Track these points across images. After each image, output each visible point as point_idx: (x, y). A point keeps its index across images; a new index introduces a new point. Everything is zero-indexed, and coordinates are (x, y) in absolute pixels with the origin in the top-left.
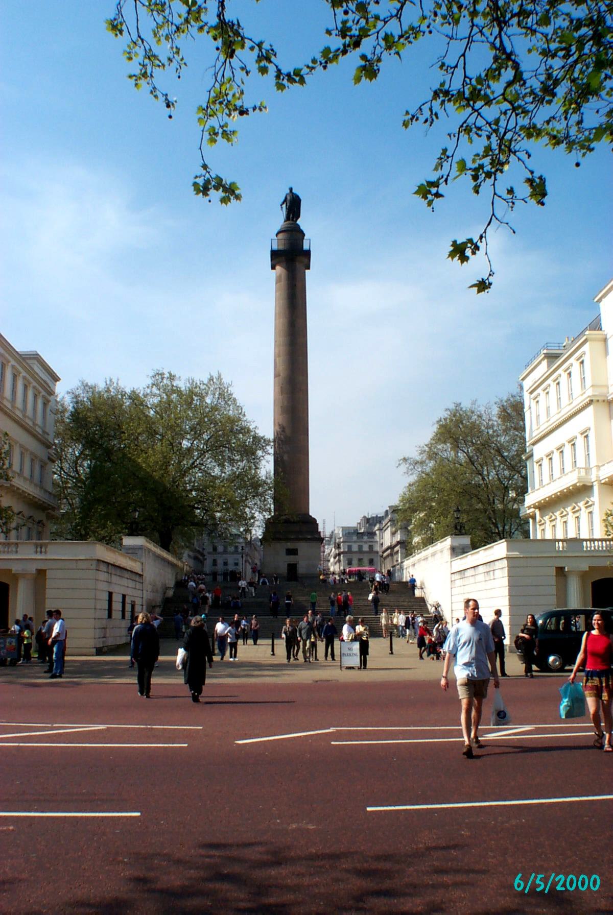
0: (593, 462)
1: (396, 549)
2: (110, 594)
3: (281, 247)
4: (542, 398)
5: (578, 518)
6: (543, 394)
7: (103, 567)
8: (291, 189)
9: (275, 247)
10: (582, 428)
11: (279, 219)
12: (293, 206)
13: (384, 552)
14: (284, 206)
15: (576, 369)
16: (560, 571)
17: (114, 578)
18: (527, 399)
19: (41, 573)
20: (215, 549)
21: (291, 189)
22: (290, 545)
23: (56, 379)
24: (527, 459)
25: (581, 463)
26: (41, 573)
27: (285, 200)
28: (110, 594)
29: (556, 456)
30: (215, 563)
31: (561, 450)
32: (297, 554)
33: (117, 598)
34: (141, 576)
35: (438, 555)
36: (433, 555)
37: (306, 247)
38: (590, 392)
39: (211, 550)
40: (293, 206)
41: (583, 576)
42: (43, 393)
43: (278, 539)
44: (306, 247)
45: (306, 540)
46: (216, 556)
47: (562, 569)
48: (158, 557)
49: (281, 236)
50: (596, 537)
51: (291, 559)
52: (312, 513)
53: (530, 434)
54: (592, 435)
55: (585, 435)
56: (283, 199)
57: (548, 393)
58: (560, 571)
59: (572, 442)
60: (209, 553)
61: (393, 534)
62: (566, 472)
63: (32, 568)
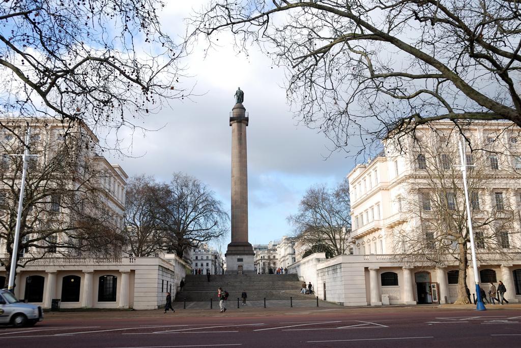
0: (382, 218)
1: (287, 258)
2: (163, 281)
3: (235, 116)
4: (358, 186)
5: (375, 243)
6: (363, 181)
7: (161, 269)
8: (239, 88)
9: (232, 116)
10: (376, 202)
11: (234, 101)
12: (240, 96)
13: (281, 259)
14: (236, 96)
15: (373, 173)
16: (366, 269)
17: (165, 274)
18: (351, 187)
19: (133, 272)
20: (197, 258)
21: (239, 88)
22: (239, 257)
23: (127, 177)
24: (352, 214)
25: (370, 219)
26: (133, 272)
27: (237, 94)
28: (163, 281)
29: (370, 211)
30: (196, 265)
31: (372, 208)
32: (242, 261)
33: (165, 283)
34: (174, 272)
35: (310, 262)
36: (308, 261)
37: (246, 116)
38: (379, 185)
39: (195, 259)
40: (240, 96)
41: (377, 271)
42: (122, 185)
43: (234, 254)
44: (246, 116)
45: (247, 254)
46: (197, 262)
47: (367, 268)
48: (182, 265)
49: (235, 111)
50: (366, 254)
51: (240, 263)
52: (250, 241)
53: (352, 204)
54: (381, 204)
55: (378, 204)
56: (235, 92)
57: (360, 184)
58: (366, 269)
59: (378, 204)
60: (194, 260)
61: (286, 250)
62: (369, 222)
63: (128, 269)
